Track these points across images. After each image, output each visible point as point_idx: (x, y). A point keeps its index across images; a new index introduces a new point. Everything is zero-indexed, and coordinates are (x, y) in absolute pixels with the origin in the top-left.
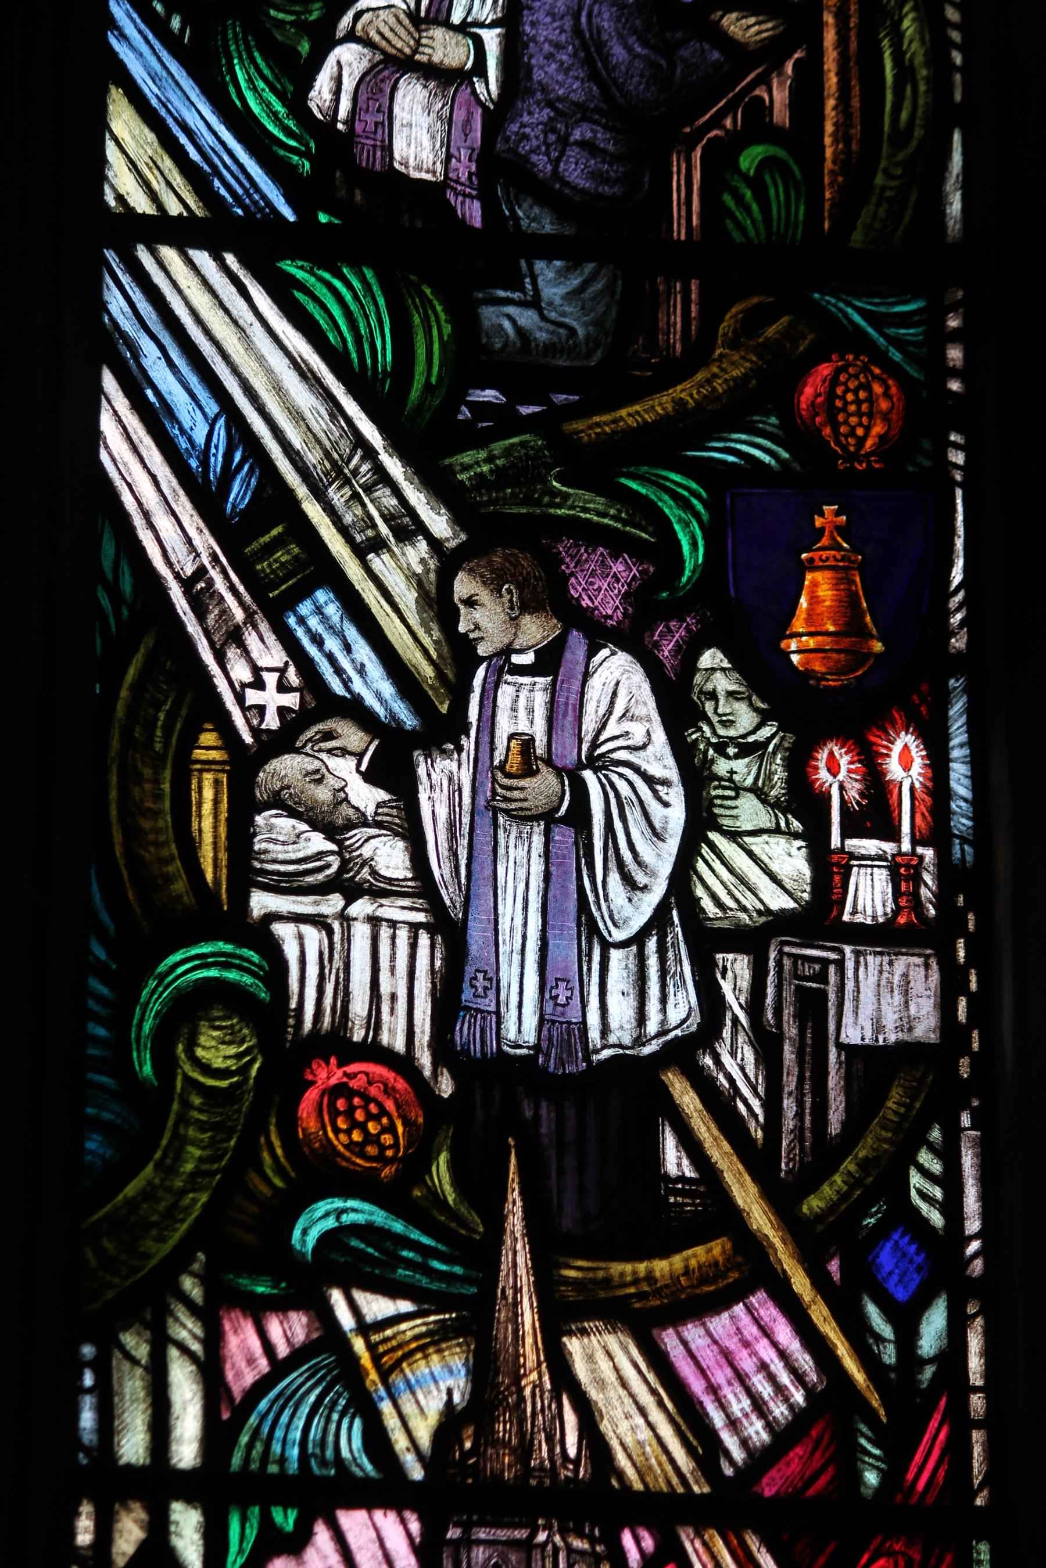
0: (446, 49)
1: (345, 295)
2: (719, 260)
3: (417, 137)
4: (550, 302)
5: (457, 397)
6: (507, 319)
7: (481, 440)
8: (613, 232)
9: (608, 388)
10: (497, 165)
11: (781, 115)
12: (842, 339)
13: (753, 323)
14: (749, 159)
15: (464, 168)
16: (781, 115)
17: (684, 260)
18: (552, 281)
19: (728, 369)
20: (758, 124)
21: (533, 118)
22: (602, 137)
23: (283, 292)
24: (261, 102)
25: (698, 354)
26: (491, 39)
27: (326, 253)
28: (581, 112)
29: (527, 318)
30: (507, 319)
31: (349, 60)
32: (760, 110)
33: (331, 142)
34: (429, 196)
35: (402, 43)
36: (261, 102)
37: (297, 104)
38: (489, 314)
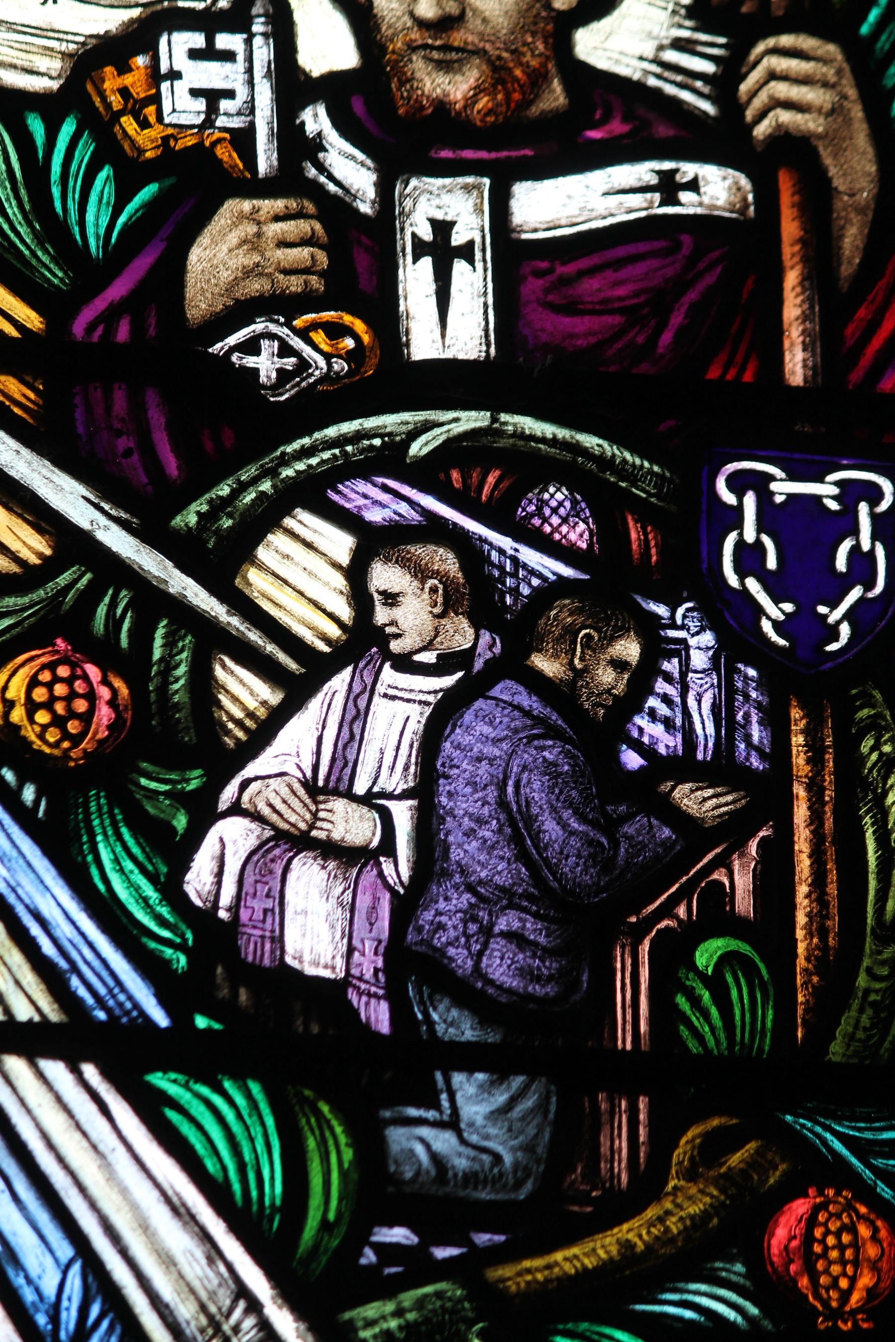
0: (350, 824)
1: (231, 1116)
2: (671, 1075)
3: (316, 927)
4: (474, 1121)
5: (358, 1236)
6: (418, 1143)
7: (388, 1289)
8: (547, 1040)
9: (544, 1221)
10: (409, 963)
11: (744, 903)
12: (816, 1170)
13: (713, 1149)
14: (707, 955)
15: (368, 963)
16: (744, 903)
17: (629, 1074)
18: (473, 1098)
19: (685, 1204)
20: (716, 914)
21: (449, 906)
22: (532, 928)
23: (152, 1109)
24: (130, 886)
25: (647, 1186)
26: (403, 814)
27: (205, 1063)
28: (508, 898)
29: (444, 1142)
30: (418, 1143)
31: (233, 837)
32: (718, 898)
33: (212, 931)
34: (329, 995)
35: (296, 816)
36: (130, 886)
37: (172, 889)
38: (398, 1138)
